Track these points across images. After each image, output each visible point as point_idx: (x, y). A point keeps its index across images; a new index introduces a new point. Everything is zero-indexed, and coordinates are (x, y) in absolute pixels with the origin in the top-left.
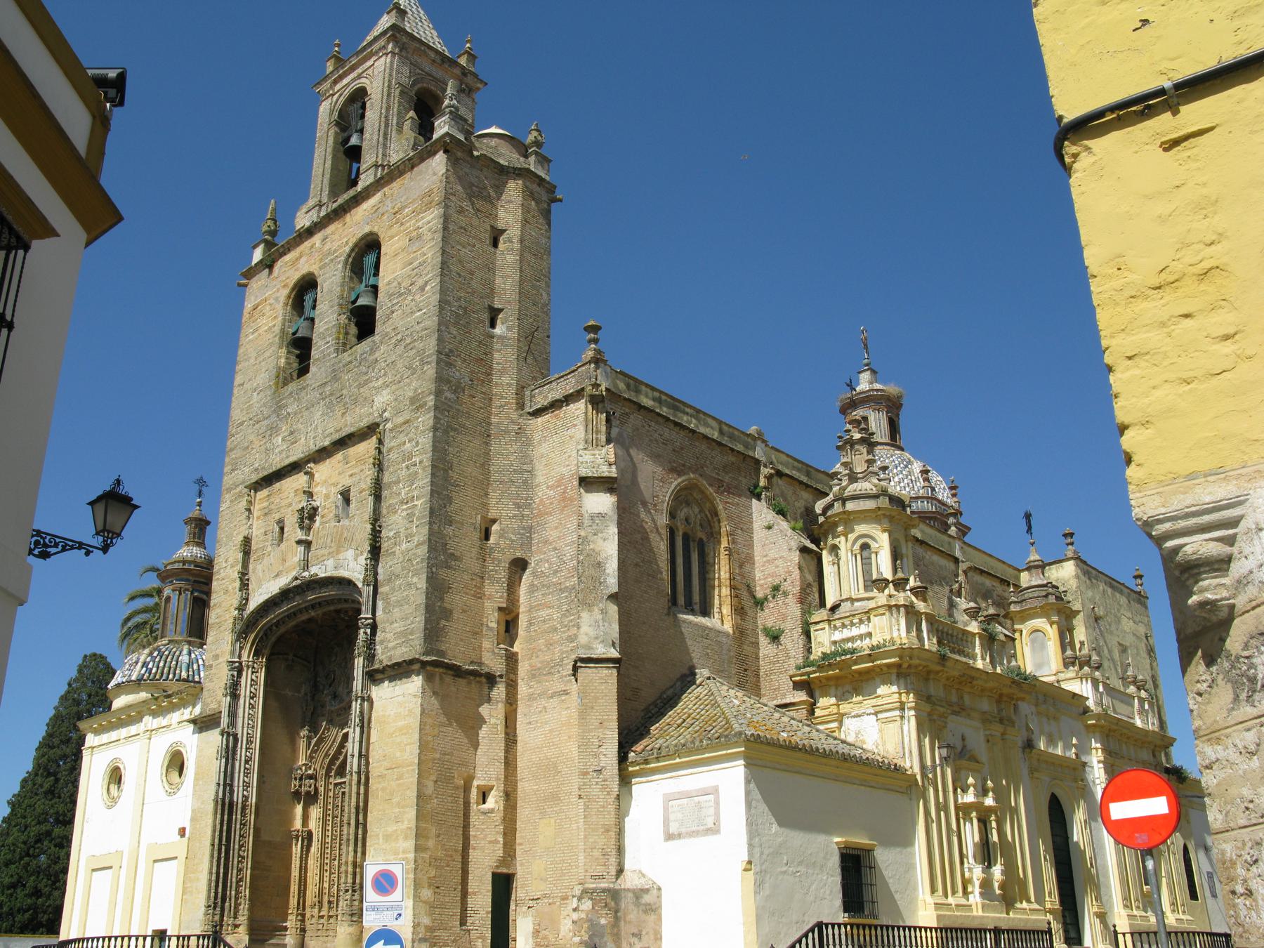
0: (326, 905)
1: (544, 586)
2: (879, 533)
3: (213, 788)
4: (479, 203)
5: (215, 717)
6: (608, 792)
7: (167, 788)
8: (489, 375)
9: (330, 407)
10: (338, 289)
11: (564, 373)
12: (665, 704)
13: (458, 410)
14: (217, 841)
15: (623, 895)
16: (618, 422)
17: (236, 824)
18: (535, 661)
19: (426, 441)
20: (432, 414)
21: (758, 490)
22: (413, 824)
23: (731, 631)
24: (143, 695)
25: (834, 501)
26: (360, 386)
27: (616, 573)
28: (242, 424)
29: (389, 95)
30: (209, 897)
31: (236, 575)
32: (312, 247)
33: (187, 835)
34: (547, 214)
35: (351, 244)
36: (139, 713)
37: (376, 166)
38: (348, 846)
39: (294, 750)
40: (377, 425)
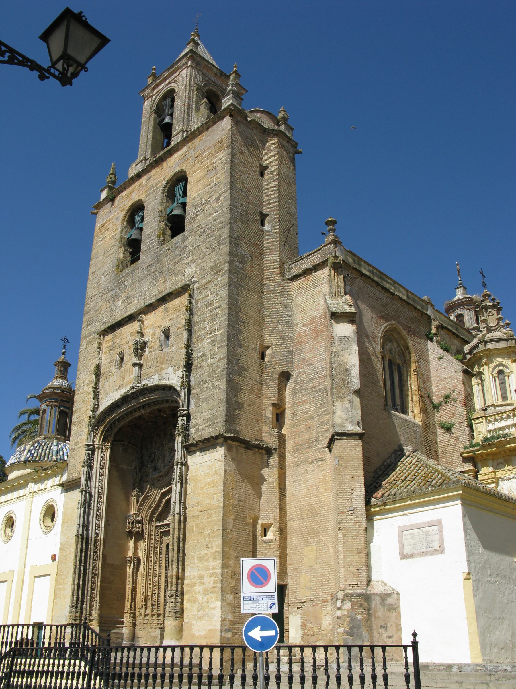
0: (149, 607)
1: (303, 389)
2: (510, 363)
3: (75, 528)
4: (252, 149)
5: (76, 481)
6: (359, 525)
7: (44, 529)
8: (261, 254)
9: (155, 279)
10: (159, 207)
11: (313, 252)
12: (386, 469)
13: (244, 274)
14: (78, 563)
15: (373, 598)
16: (349, 283)
17: (90, 552)
18: (297, 439)
19: (224, 292)
20: (227, 275)
21: (431, 336)
22: (220, 549)
23: (420, 423)
24: (28, 470)
25: (479, 343)
26: (175, 264)
27: (358, 376)
28: (94, 296)
29: (190, 90)
30: (73, 600)
31: (91, 390)
32: (140, 185)
33: (57, 560)
34: (293, 160)
35: (167, 179)
36: (25, 481)
37: (183, 131)
38: (172, 564)
39: (128, 504)
40: (189, 286)
